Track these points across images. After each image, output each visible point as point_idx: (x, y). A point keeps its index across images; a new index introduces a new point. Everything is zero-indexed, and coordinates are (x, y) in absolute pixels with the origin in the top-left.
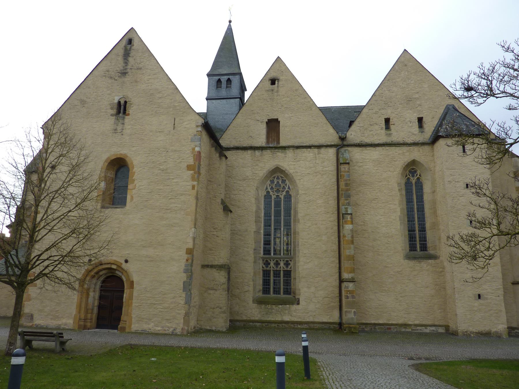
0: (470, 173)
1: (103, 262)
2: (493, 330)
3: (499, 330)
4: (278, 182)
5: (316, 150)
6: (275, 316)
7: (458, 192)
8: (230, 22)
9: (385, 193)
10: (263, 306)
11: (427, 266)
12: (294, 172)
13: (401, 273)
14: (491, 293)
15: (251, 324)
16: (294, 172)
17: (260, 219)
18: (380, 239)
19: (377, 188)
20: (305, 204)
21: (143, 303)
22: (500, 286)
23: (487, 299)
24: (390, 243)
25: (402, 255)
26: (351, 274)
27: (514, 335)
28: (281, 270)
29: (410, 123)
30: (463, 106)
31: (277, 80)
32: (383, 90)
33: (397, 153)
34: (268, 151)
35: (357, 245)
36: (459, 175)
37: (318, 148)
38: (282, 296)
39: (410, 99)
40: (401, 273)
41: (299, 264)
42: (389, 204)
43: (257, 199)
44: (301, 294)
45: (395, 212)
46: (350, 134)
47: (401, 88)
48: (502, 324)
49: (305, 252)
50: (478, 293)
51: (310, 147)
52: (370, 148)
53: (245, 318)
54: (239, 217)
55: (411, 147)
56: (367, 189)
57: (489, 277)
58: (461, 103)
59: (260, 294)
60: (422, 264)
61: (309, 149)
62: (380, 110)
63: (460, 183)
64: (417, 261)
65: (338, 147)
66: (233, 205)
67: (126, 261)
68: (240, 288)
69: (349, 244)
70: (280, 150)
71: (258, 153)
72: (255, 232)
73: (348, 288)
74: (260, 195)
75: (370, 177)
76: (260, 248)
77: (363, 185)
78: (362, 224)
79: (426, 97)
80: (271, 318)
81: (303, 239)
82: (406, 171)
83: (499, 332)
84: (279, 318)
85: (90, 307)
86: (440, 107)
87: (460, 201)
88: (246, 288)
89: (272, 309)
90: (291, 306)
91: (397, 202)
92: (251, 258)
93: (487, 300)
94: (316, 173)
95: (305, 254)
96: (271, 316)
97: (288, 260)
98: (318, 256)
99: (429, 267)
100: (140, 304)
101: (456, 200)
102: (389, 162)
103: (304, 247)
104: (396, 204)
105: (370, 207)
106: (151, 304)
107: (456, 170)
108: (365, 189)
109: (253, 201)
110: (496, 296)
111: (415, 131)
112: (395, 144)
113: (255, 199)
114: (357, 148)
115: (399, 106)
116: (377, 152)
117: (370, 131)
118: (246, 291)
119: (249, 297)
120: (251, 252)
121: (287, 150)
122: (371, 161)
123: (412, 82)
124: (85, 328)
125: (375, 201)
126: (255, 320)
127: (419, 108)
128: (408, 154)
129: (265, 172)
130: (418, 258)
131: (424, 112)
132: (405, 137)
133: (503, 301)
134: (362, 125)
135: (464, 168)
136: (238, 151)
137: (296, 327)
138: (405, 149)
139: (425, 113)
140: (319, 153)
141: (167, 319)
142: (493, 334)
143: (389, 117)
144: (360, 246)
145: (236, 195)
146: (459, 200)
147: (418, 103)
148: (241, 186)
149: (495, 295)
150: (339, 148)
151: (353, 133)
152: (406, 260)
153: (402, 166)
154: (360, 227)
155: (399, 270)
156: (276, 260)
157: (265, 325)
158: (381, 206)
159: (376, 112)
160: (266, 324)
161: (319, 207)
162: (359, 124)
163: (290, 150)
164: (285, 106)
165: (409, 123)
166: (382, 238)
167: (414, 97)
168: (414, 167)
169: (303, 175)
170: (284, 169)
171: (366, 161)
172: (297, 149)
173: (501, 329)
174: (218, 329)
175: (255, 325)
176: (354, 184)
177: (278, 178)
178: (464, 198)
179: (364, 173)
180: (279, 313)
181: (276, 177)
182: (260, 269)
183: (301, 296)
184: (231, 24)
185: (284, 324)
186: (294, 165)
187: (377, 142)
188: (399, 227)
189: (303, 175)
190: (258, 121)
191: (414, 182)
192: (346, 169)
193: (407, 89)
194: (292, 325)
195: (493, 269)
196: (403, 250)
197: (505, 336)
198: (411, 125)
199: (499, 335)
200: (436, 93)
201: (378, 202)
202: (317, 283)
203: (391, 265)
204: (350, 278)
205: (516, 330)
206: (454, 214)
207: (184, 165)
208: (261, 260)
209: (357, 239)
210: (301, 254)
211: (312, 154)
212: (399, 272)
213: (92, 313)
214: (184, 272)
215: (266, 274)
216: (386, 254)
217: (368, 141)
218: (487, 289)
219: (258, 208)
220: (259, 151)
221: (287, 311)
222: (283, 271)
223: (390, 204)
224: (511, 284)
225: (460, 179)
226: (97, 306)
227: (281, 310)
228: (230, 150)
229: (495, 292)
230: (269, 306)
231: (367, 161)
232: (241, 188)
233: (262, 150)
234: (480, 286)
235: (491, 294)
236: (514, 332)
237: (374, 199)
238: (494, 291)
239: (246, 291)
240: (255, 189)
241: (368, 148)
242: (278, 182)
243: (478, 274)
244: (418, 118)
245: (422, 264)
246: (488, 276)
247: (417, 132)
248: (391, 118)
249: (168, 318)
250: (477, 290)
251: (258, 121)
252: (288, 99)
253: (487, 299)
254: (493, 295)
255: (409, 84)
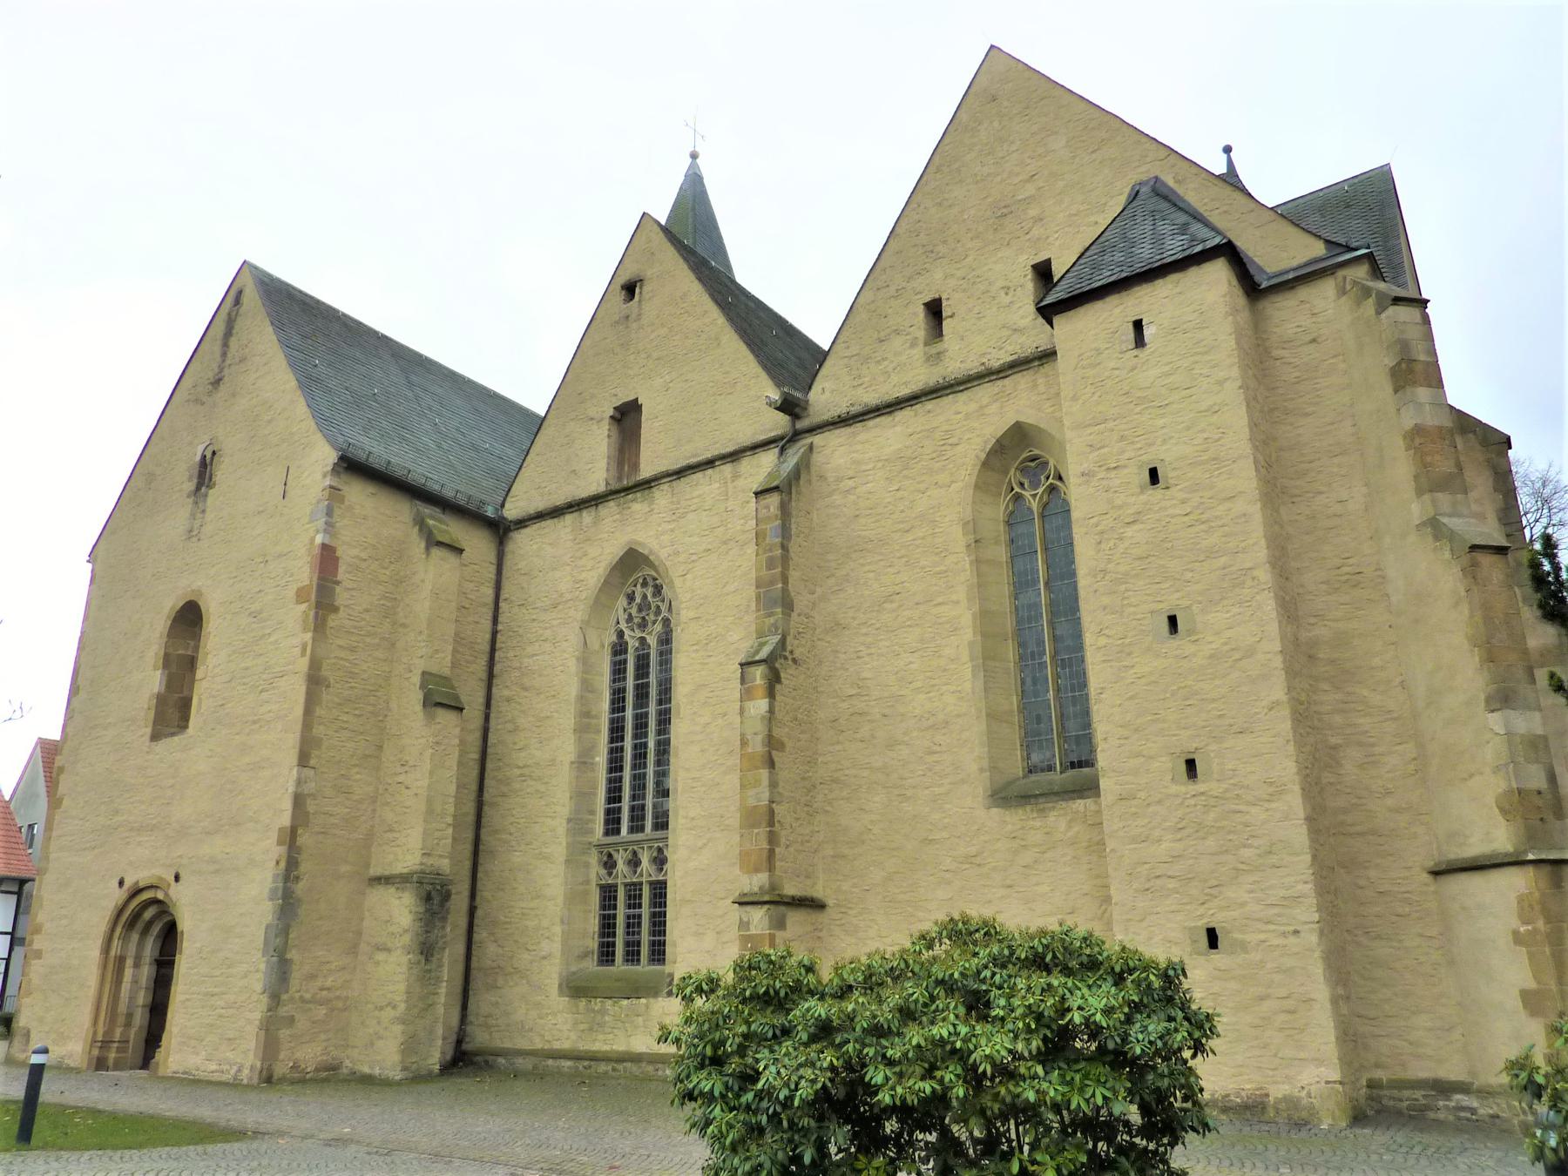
0: (1160, 422)
1: (142, 884)
2: (1277, 1091)
3: (1304, 1094)
4: (645, 597)
5: (727, 469)
6: (611, 1036)
7: (1120, 507)
8: (694, 156)
9: (923, 568)
10: (583, 1003)
11: (1069, 827)
12: (669, 555)
13: (978, 860)
14: (1258, 920)
15: (550, 1062)
16: (669, 555)
17: (594, 721)
18: (906, 739)
19: (898, 555)
20: (697, 651)
21: (193, 994)
22: (1300, 887)
23: (1243, 947)
24: (938, 749)
25: (980, 790)
26: (759, 875)
27: (1451, 1118)
28: (641, 884)
29: (1007, 294)
30: (1194, 170)
31: (638, 284)
32: (922, 207)
33: (959, 416)
34: (612, 504)
35: (837, 770)
36: (1122, 438)
37: (732, 462)
38: (620, 966)
39: (1005, 211)
40: (978, 860)
41: (676, 857)
42: (936, 605)
43: (585, 662)
44: (679, 960)
45: (955, 630)
46: (820, 391)
47: (977, 182)
48: (1319, 1062)
49: (692, 814)
50: (1203, 923)
51: (709, 463)
52: (878, 420)
53: (539, 1044)
54: (538, 724)
55: (1006, 381)
56: (869, 564)
57: (1250, 846)
58: (1186, 162)
59: (591, 965)
60: (1052, 819)
61: (710, 471)
62: (909, 279)
63: (1126, 471)
64: (1032, 811)
65: (781, 444)
66: (526, 689)
67: (177, 878)
68: (531, 948)
69: (757, 768)
70: (639, 495)
71: (587, 516)
72: (572, 763)
73: (749, 930)
74: (596, 646)
75: (877, 521)
76: (592, 812)
77: (854, 556)
78: (854, 692)
79: (1061, 184)
80: (599, 1045)
81: (687, 770)
82: (1006, 472)
83: (1304, 1102)
84: (620, 1046)
85: (122, 1008)
86: (1110, 204)
87: (1127, 544)
88: (546, 947)
89: (603, 1012)
90: (652, 1000)
91: (961, 594)
92: (559, 850)
93: (1247, 952)
94: (725, 543)
95: (693, 819)
96: (601, 1037)
97: (661, 845)
98: (727, 822)
99: (1076, 829)
100: (188, 997)
101: (1111, 544)
102: (934, 455)
103: (692, 795)
104: (958, 602)
105: (878, 626)
106: (206, 994)
107: (1111, 424)
108: (863, 565)
109: (573, 666)
110: (1284, 934)
111: (1022, 318)
112: (951, 386)
113: (578, 659)
114: (837, 432)
115: (969, 245)
116: (898, 429)
117: (879, 362)
118: (544, 958)
119: (551, 974)
120: (561, 826)
121: (654, 490)
122: (880, 464)
123: (1014, 148)
124: (100, 1064)
125: (892, 602)
126: (561, 1050)
127: (1035, 232)
128: (994, 407)
129: (601, 571)
130: (1036, 796)
131: (1051, 239)
132: (989, 350)
133: (1317, 954)
134: (854, 350)
135: (1138, 409)
136: (543, 524)
137: (660, 1073)
138: (985, 392)
139: (1057, 243)
140: (736, 477)
141: (230, 1039)
142: (1277, 1111)
143: (937, 296)
144: (847, 772)
145: (536, 655)
146: (1121, 539)
147: (1033, 212)
148: (546, 629)
149: (1282, 928)
150: (783, 447)
151: (827, 385)
152: (995, 810)
153: (977, 457)
154: (845, 705)
155: (973, 850)
156: (631, 848)
157: (585, 1067)
158: (909, 619)
159: (897, 290)
160: (586, 1063)
161: (732, 657)
162: (848, 347)
163: (662, 487)
164: (655, 355)
165: (1002, 293)
166: (915, 734)
167: (1020, 198)
168: (1036, 452)
169: (694, 557)
170: (646, 552)
171: (864, 467)
172: (679, 478)
173: (1313, 1088)
174: (386, 1072)
175: (558, 1067)
176: (830, 557)
177: (645, 584)
178: (1141, 526)
179: (857, 513)
180: (620, 1024)
181: (641, 581)
182: (587, 882)
183: (677, 965)
184: (698, 161)
185: (628, 1065)
186: (672, 530)
187: (904, 392)
188: (968, 686)
189: (694, 557)
190: (592, 419)
191: (1035, 505)
192: (772, 509)
193: (999, 178)
194: (650, 1068)
195: (1267, 810)
196: (981, 770)
197: (1330, 1118)
198: (1007, 300)
199: (1304, 1114)
200: (1094, 156)
201: (900, 606)
202: (721, 917)
203: (945, 834)
204: (756, 889)
205: (1458, 1097)
206: (1106, 600)
207: (291, 593)
208: (594, 852)
209: (838, 747)
210: (683, 821)
211: (717, 485)
212: (973, 860)
213: (128, 1024)
214: (271, 899)
215: (608, 895)
216: (927, 792)
217: (871, 398)
218: (1243, 905)
219: (587, 686)
220: (590, 509)
221: (640, 1018)
222: (651, 883)
223: (939, 604)
224: (1426, 877)
225: (1127, 455)
226: (144, 1006)
227: (627, 1015)
228: (526, 526)
229: (1279, 915)
230: (597, 1004)
231: (868, 468)
232: (548, 633)
233: (597, 505)
234: (1213, 891)
235: (1260, 926)
236: (1447, 1107)
237: (888, 598)
238: (1276, 910)
239: (544, 958)
240: (577, 630)
241: (871, 423)
242: (645, 597)
243: (1204, 838)
244: (1032, 266)
245: (1052, 817)
246: (1245, 846)
247: (1030, 318)
248: (944, 297)
249: (231, 1036)
250: (1201, 910)
251: (592, 419)
252: (663, 331)
253: (1243, 947)
254: (1272, 927)
255: (1003, 158)
